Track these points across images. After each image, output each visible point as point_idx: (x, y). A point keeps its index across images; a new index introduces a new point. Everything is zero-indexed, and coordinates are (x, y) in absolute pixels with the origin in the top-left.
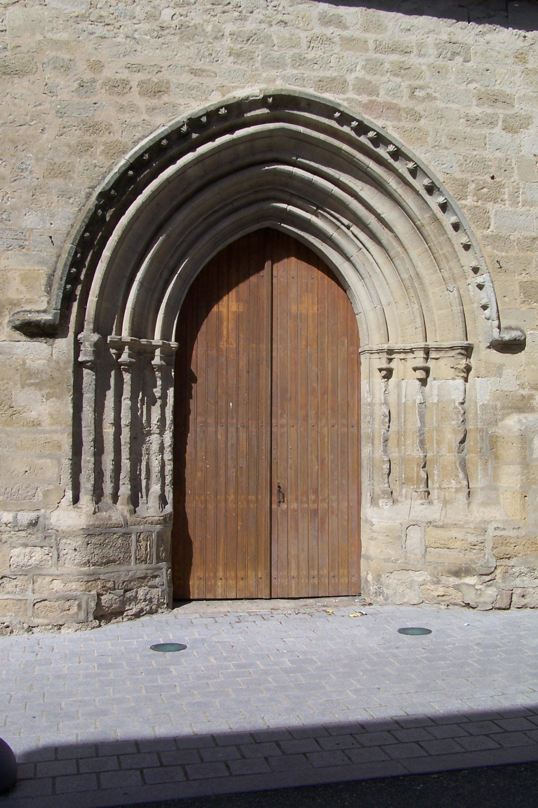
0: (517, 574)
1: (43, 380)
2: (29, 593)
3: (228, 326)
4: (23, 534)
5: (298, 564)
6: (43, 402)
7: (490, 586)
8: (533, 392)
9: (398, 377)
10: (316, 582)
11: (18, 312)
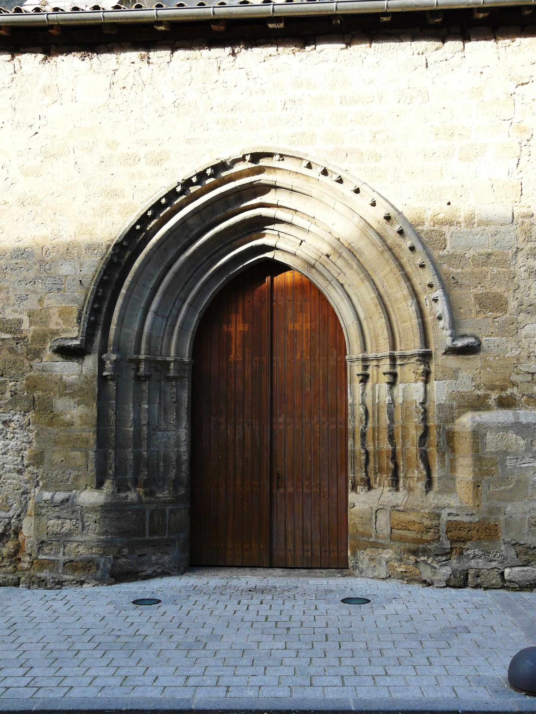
0: (471, 556)
1: (75, 391)
2: (61, 555)
3: (236, 342)
4: (57, 509)
5: (294, 539)
6: (75, 407)
7: (446, 565)
8: (489, 392)
9: (372, 382)
10: (310, 555)
11: (57, 339)
